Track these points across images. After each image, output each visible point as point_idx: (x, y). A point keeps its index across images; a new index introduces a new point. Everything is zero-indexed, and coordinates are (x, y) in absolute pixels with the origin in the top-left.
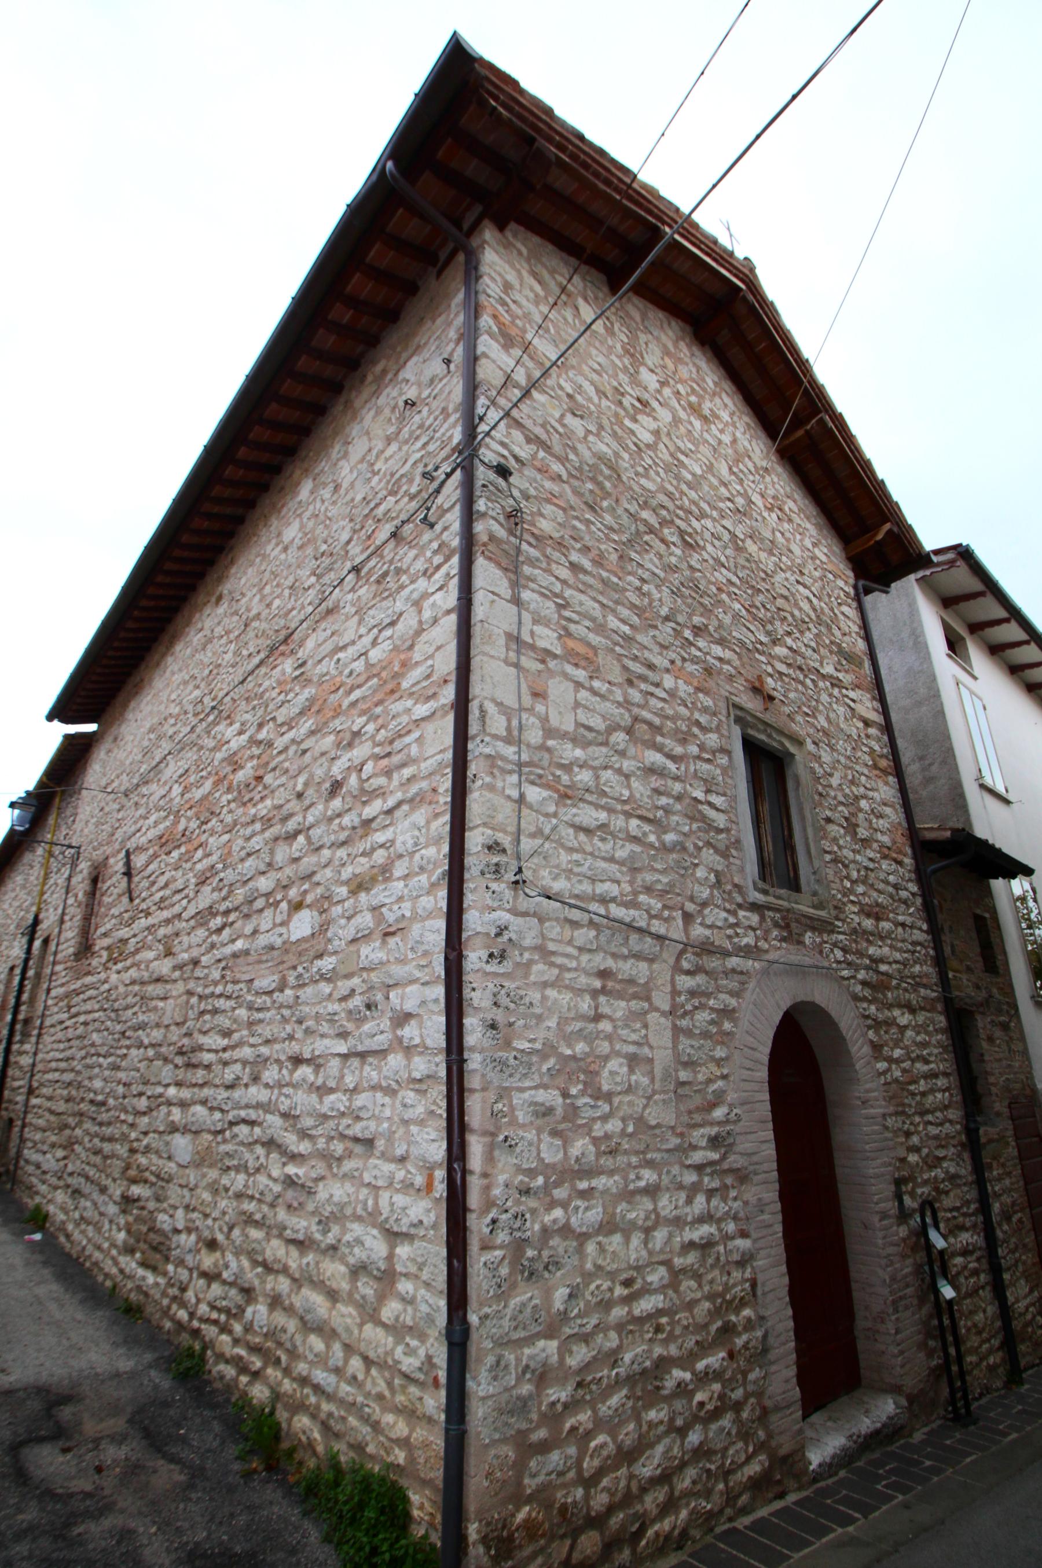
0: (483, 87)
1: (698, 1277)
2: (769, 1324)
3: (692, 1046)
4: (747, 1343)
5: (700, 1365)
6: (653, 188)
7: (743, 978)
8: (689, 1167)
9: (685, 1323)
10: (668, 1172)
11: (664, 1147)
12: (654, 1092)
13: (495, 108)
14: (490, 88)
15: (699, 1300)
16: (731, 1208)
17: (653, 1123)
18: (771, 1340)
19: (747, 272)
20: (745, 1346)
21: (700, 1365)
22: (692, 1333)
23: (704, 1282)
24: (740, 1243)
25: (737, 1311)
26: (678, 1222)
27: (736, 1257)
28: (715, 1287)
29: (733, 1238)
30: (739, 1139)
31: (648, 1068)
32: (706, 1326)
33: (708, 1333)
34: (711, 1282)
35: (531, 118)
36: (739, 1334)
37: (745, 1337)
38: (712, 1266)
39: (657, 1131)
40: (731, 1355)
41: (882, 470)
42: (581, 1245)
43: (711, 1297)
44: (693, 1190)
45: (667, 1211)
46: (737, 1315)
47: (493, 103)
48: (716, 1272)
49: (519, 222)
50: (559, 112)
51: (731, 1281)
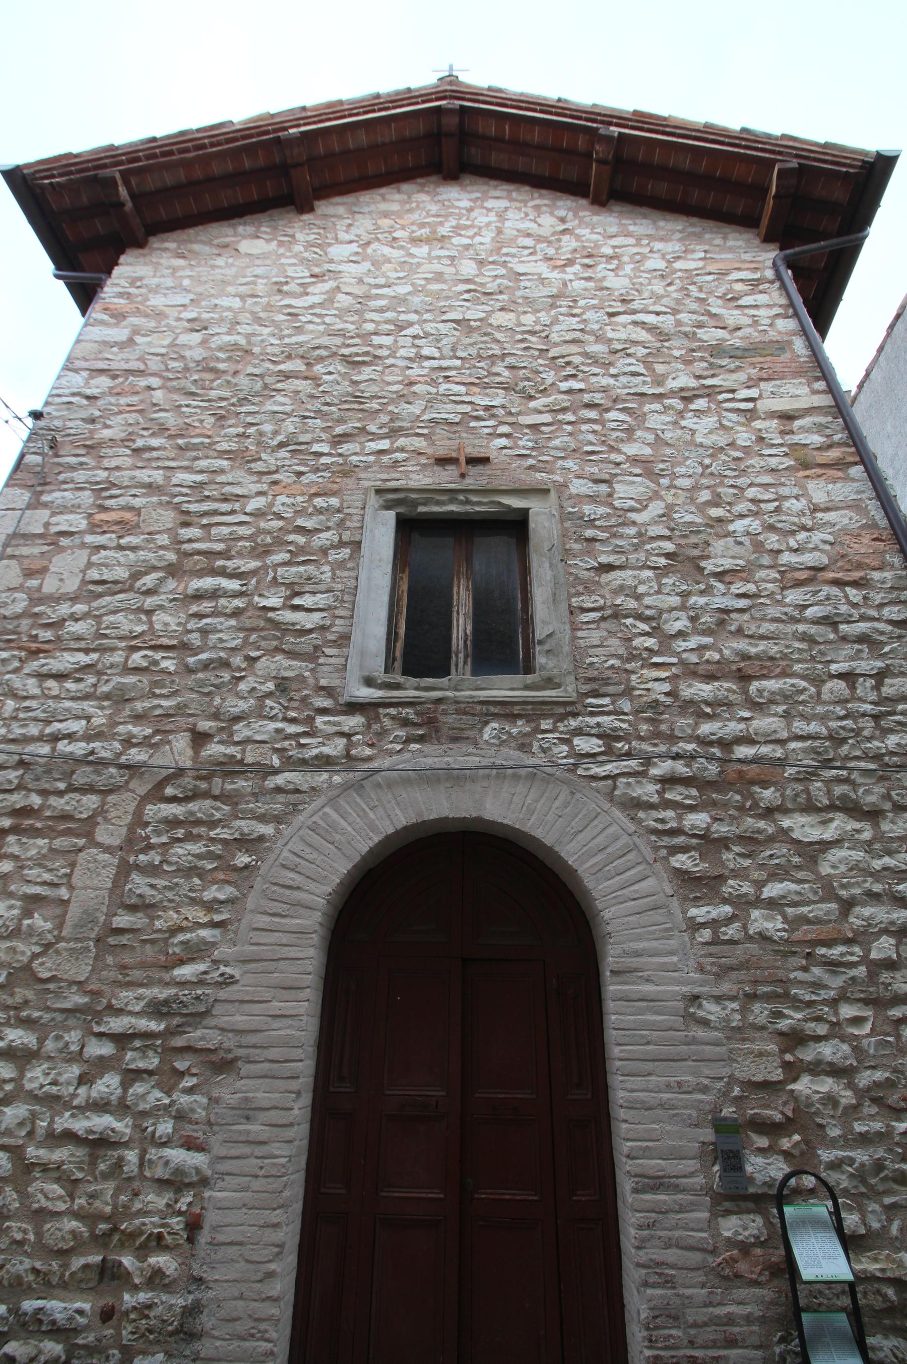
0: (37, 179)
1: (72, 1185)
2: (211, 1294)
3: (152, 886)
4: (149, 1307)
5: (29, 1305)
6: (330, 105)
7: (292, 798)
8: (101, 1035)
9: (19, 1236)
10: (58, 1038)
11: (59, 1006)
12: (59, 939)
13: (51, 183)
14: (42, 175)
15: (58, 1214)
16: (173, 1103)
17: (46, 975)
18: (206, 1321)
19: (450, 88)
20: (144, 1309)
21: (29, 1305)
22: (28, 1255)
23: (78, 1192)
24: (177, 1155)
25: (142, 1252)
26: (54, 1102)
27: (160, 1172)
28: (97, 1203)
29: (164, 1144)
30: (218, 1009)
31: (58, 911)
32: (64, 1254)
33: (65, 1266)
34: (93, 1196)
35: (252, 131)
36: (136, 1288)
37: (143, 1297)
38: (105, 1176)
39: (51, 986)
40: (107, 1315)
41: (733, 122)
42: (181, 1325)
43: (89, 1217)
44: (102, 1065)
45: (35, 1085)
46: (142, 1258)
47: (46, 181)
48: (109, 1187)
49: (319, 198)
50: (159, 134)
51: (138, 1206)
